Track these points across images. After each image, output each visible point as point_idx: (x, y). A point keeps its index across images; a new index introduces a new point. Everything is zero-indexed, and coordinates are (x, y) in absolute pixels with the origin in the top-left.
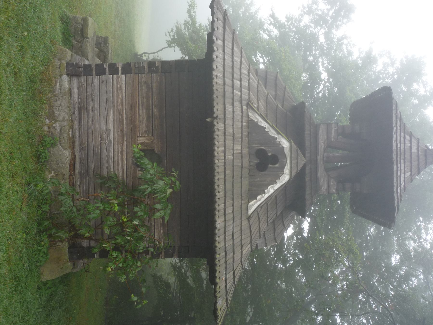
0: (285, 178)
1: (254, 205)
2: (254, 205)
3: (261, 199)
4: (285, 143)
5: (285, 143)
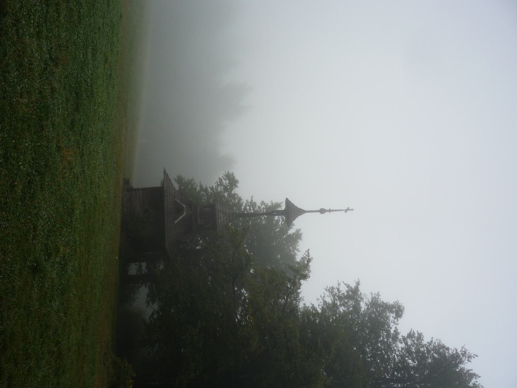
0: (184, 214)
1: (176, 222)
2: (176, 222)
3: (178, 220)
4: (184, 206)
5: (184, 206)
